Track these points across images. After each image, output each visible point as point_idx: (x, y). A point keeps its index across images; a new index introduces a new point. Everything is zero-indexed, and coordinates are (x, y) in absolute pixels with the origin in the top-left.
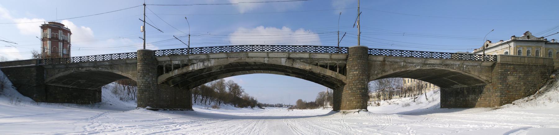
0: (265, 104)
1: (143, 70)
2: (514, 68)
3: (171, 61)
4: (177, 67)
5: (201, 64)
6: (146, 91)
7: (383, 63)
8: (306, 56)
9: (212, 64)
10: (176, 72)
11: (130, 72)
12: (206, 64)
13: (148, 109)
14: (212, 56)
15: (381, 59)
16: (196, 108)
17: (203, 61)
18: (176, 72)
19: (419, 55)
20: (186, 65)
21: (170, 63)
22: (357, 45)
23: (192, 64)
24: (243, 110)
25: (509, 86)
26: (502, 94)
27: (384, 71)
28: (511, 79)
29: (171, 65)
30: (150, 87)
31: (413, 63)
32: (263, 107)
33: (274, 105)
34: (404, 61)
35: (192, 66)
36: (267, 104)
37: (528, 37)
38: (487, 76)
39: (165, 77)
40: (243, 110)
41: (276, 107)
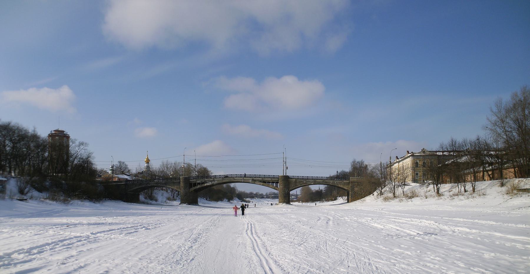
0: (251, 193)
1: (184, 186)
2: (358, 184)
3: (196, 181)
4: (199, 184)
5: (211, 183)
6: (185, 196)
7: (296, 182)
8: (261, 179)
9: (216, 183)
10: (199, 186)
11: (176, 186)
12: (213, 183)
13: (187, 204)
14: (215, 179)
15: (294, 180)
16: (200, 204)
17: (211, 181)
18: (199, 186)
19: (311, 178)
20: (204, 183)
21: (195, 182)
22: (282, 175)
23: (206, 183)
24: (219, 204)
25: (355, 193)
26: (352, 197)
27: (297, 185)
28: (356, 189)
29: (196, 183)
30: (187, 194)
31: (310, 182)
32: (247, 199)
33: (264, 194)
34: (305, 181)
35: (206, 183)
36: (255, 193)
37: (424, 152)
38: (347, 187)
39: (193, 189)
40: (219, 204)
41: (269, 198)
